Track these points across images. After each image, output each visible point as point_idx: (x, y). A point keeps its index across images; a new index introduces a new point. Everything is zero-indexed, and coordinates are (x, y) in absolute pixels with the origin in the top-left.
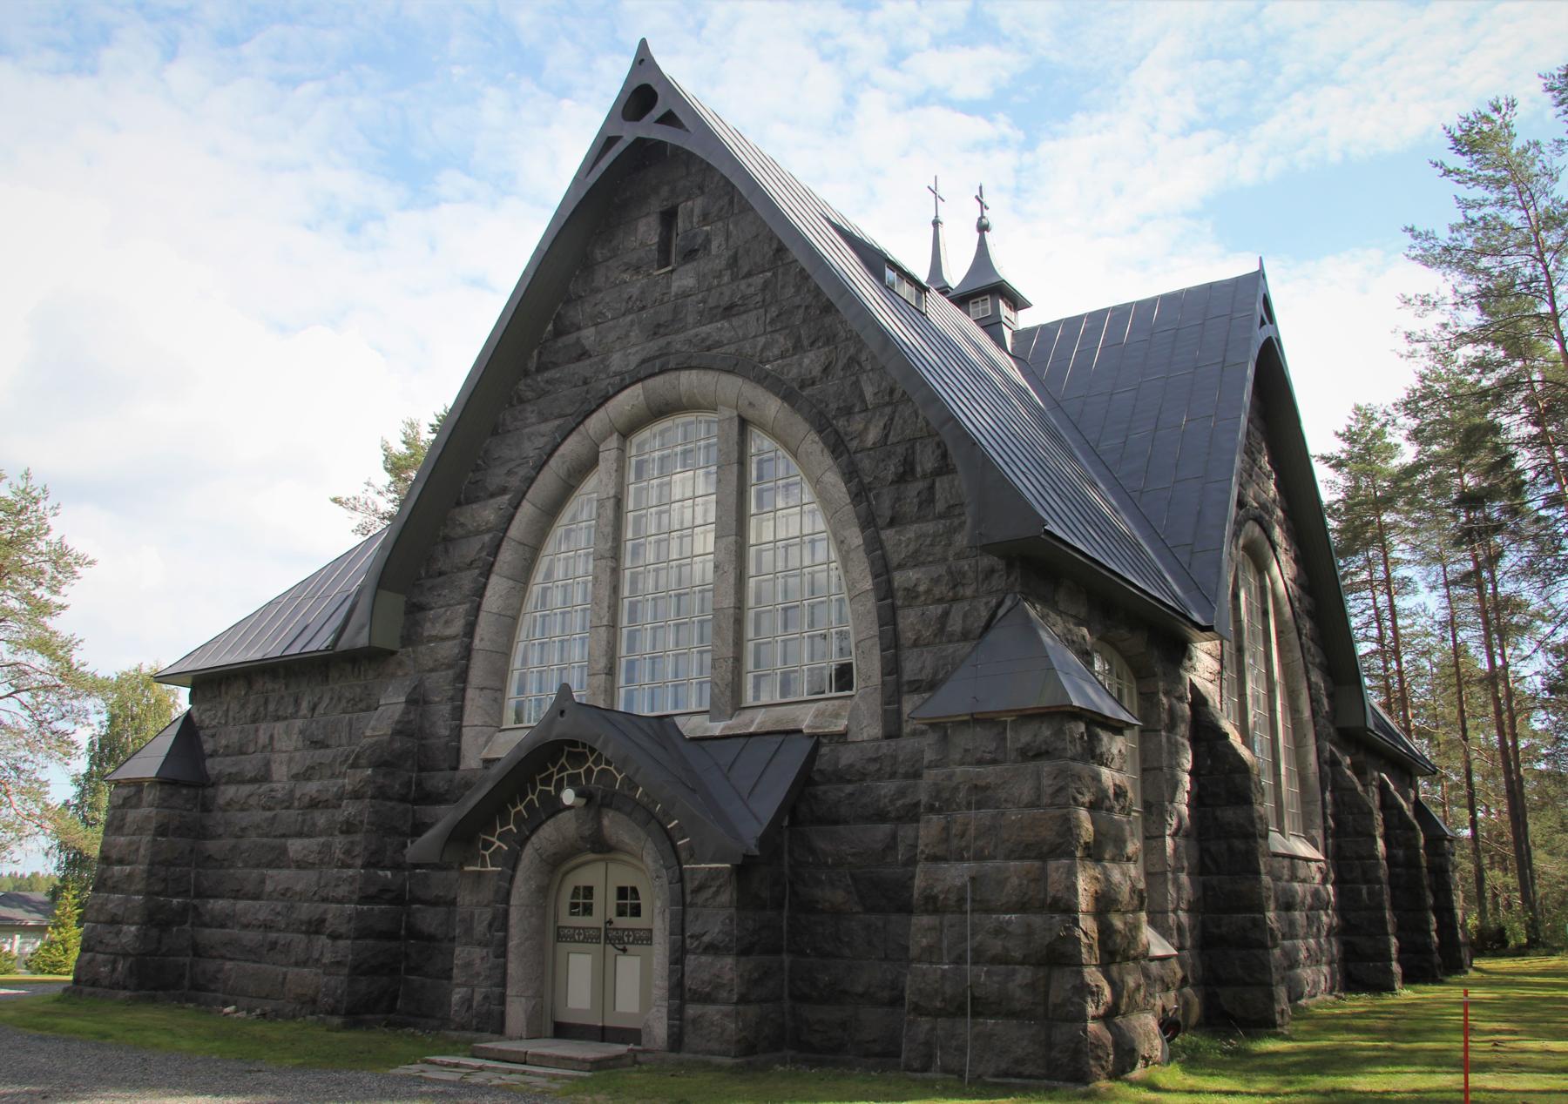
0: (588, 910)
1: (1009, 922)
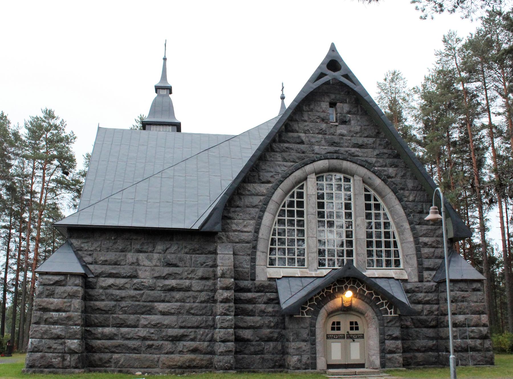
0: (339, 329)
1: (474, 329)
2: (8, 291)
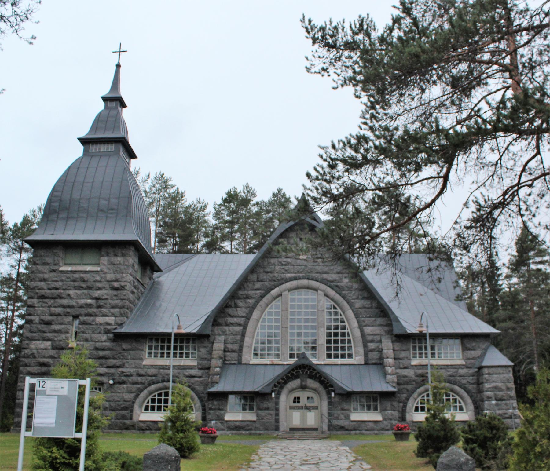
0: (299, 402)
2: (538, 139)
